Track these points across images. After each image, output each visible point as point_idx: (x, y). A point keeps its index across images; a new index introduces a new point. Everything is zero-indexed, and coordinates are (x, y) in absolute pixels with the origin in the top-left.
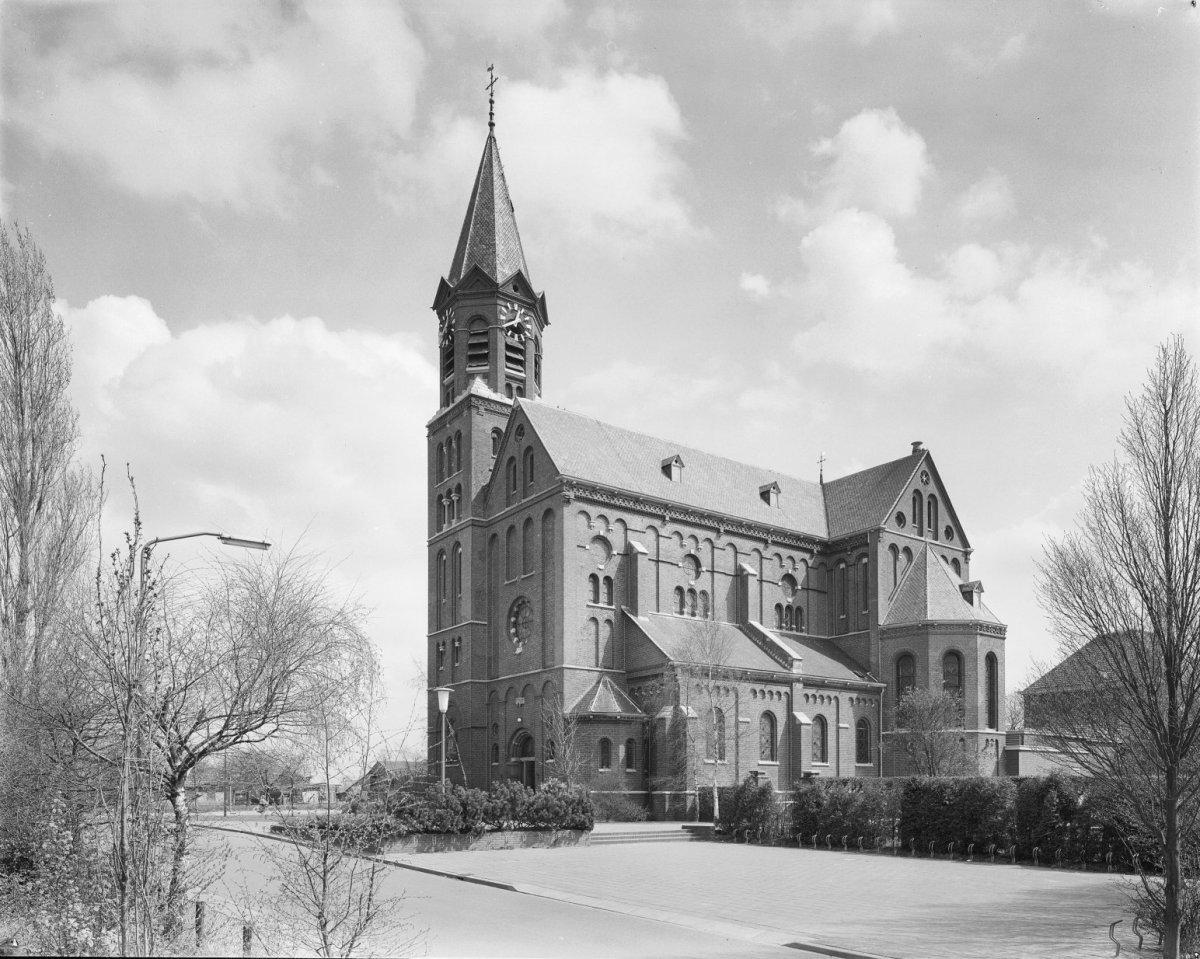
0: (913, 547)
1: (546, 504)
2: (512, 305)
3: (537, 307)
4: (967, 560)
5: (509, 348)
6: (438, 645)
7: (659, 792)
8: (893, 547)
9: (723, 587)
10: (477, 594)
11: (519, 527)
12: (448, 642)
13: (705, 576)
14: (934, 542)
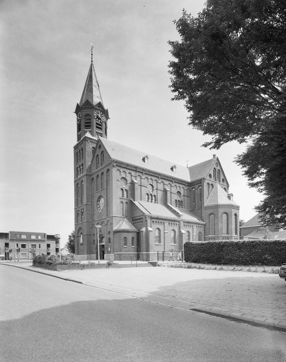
0: (214, 184)
1: (107, 168)
2: (98, 111)
3: (105, 113)
4: (228, 188)
5: (97, 124)
6: (77, 211)
7: (142, 253)
8: (208, 184)
9: (160, 195)
10: (88, 195)
11: (100, 175)
12: (80, 210)
13: (155, 191)
14: (219, 183)
